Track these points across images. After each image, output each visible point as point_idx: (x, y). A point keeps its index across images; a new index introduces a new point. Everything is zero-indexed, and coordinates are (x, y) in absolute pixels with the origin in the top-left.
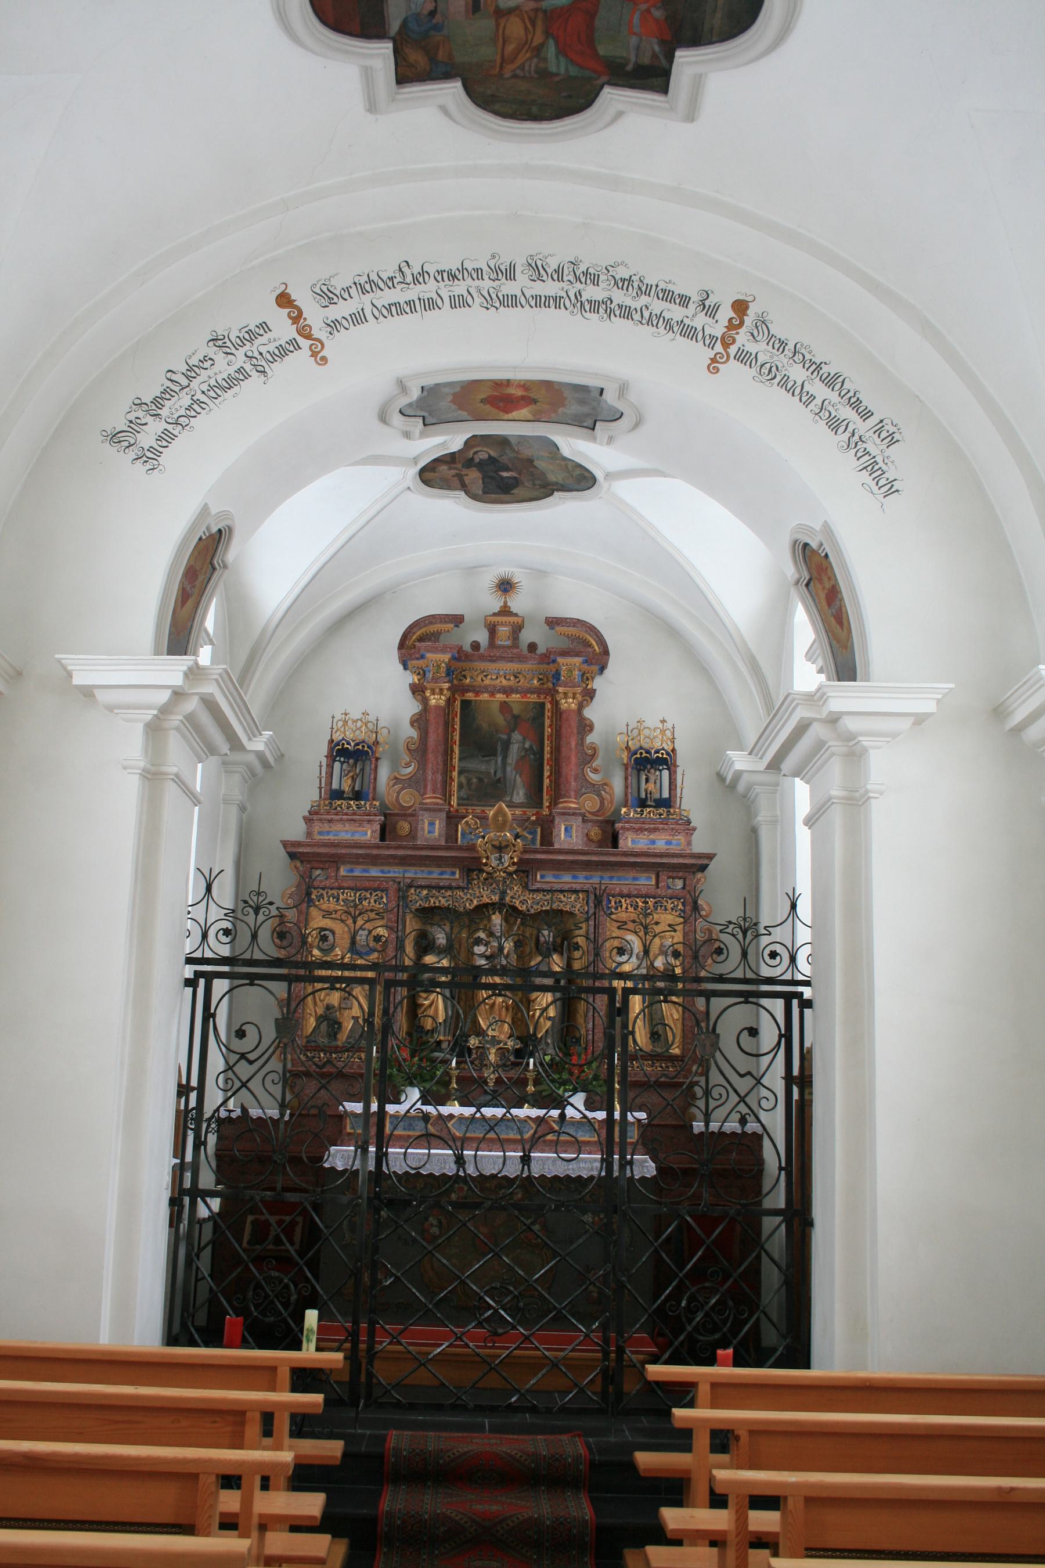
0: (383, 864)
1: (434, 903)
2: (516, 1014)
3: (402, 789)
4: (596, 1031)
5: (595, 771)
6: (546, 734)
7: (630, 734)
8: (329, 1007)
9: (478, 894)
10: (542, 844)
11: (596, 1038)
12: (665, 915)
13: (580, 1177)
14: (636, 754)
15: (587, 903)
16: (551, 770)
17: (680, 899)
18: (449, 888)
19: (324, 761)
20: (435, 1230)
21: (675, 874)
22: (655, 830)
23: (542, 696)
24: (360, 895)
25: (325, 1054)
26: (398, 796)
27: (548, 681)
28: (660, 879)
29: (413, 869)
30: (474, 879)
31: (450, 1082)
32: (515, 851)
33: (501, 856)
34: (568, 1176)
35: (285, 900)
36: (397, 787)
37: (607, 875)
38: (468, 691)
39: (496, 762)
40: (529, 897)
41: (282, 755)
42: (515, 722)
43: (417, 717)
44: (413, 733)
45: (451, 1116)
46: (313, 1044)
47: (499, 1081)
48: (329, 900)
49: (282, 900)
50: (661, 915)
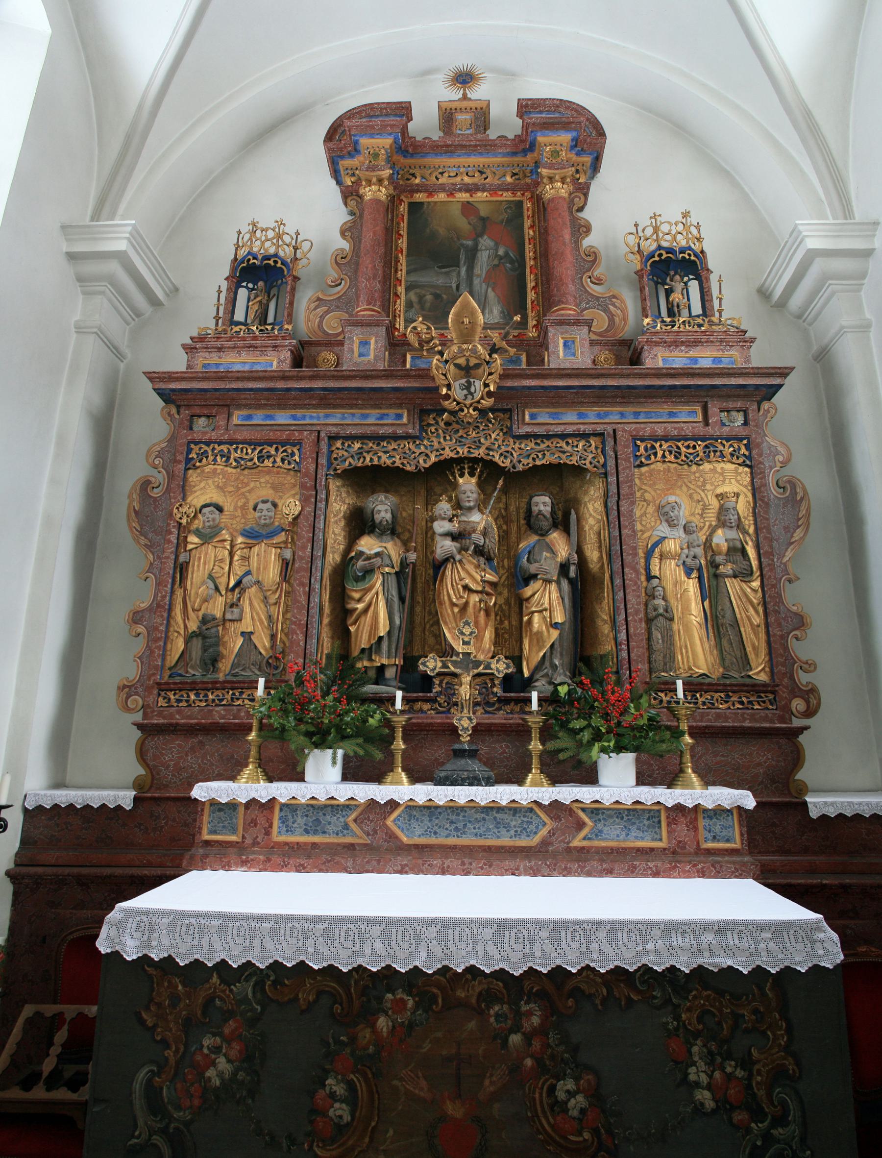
0: (295, 407)
1: (371, 460)
2: (501, 622)
3: (327, 312)
4: (632, 644)
5: (598, 282)
6: (526, 238)
7: (641, 234)
8: (205, 620)
9: (436, 445)
10: (529, 363)
11: (632, 655)
12: (722, 465)
13: (673, 969)
14: (653, 257)
15: (603, 452)
16: (536, 280)
17: (741, 440)
18: (395, 438)
19: (224, 285)
20: (340, 1111)
21: (731, 405)
22: (696, 343)
23: (519, 193)
24: (261, 451)
25: (197, 695)
26: (321, 322)
27: (525, 176)
28: (710, 412)
29: (338, 412)
30: (429, 425)
31: (391, 739)
32: (490, 374)
33: (469, 383)
34: (646, 969)
35: (150, 460)
36: (320, 311)
37: (629, 410)
38: (418, 191)
39: (459, 273)
40: (512, 445)
41: (177, 290)
42: (484, 224)
43: (349, 225)
44: (345, 245)
45: (392, 804)
46: (178, 679)
47: (478, 731)
48: (215, 460)
49: (147, 461)
50: (716, 465)
